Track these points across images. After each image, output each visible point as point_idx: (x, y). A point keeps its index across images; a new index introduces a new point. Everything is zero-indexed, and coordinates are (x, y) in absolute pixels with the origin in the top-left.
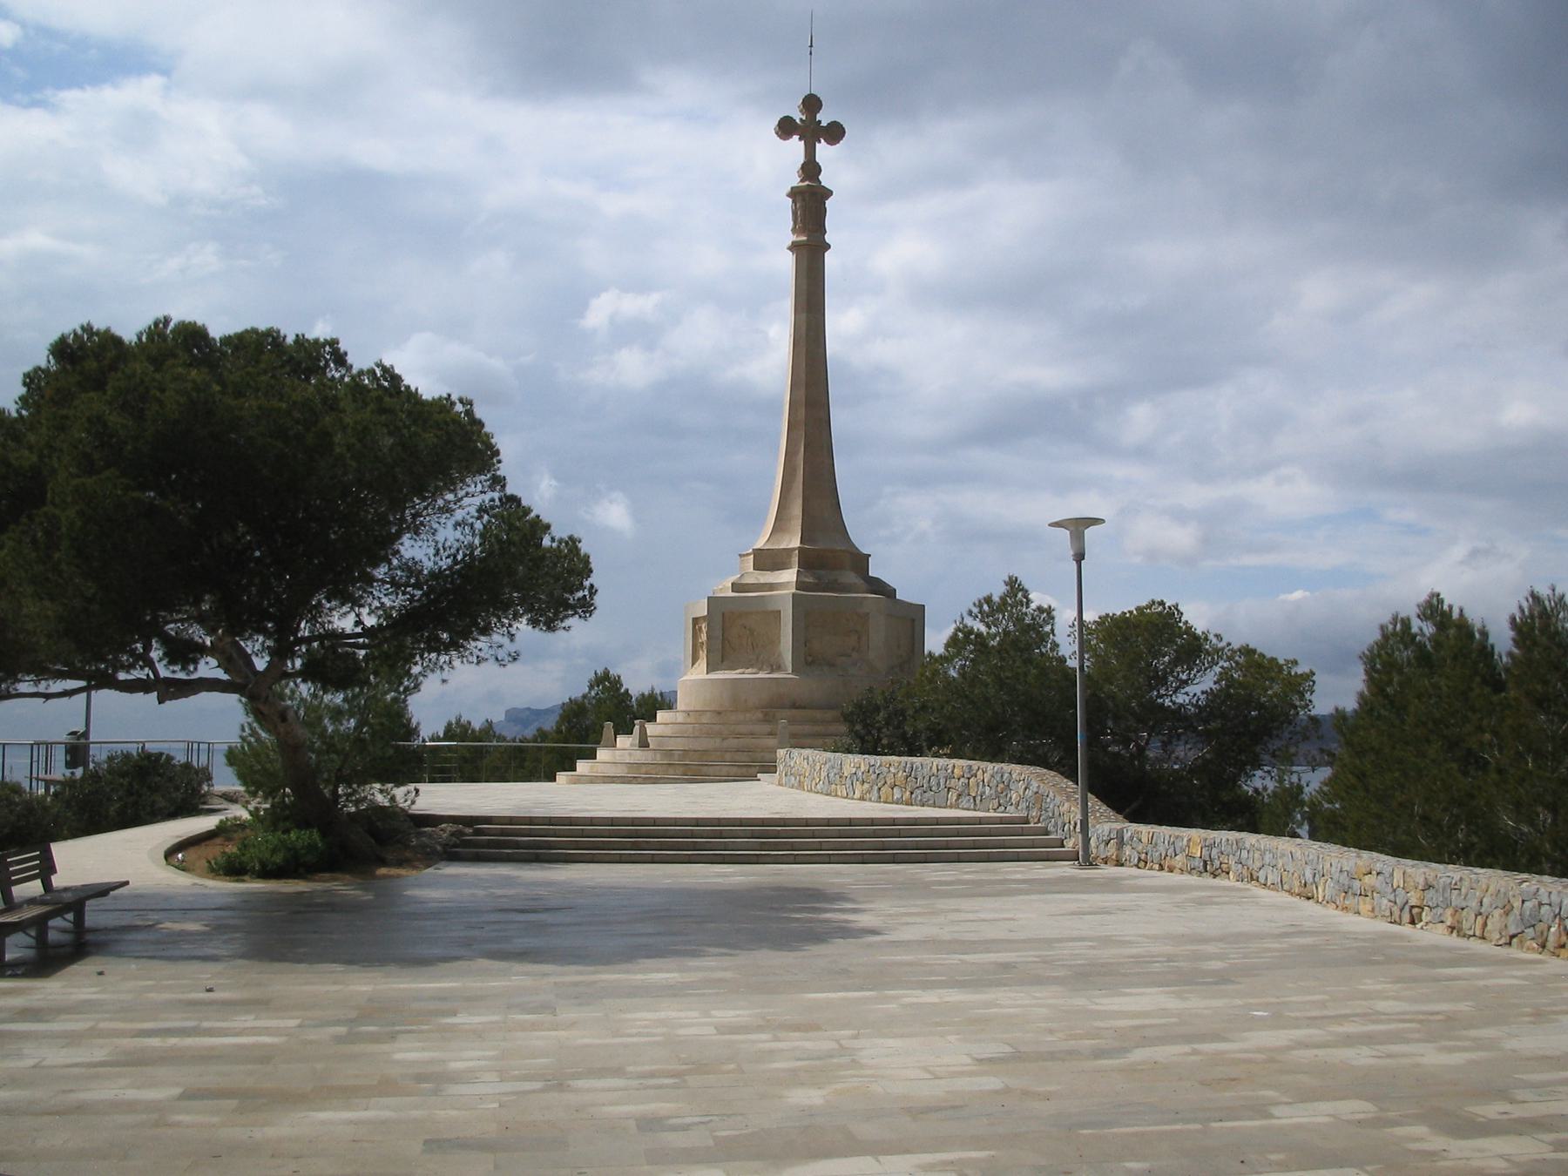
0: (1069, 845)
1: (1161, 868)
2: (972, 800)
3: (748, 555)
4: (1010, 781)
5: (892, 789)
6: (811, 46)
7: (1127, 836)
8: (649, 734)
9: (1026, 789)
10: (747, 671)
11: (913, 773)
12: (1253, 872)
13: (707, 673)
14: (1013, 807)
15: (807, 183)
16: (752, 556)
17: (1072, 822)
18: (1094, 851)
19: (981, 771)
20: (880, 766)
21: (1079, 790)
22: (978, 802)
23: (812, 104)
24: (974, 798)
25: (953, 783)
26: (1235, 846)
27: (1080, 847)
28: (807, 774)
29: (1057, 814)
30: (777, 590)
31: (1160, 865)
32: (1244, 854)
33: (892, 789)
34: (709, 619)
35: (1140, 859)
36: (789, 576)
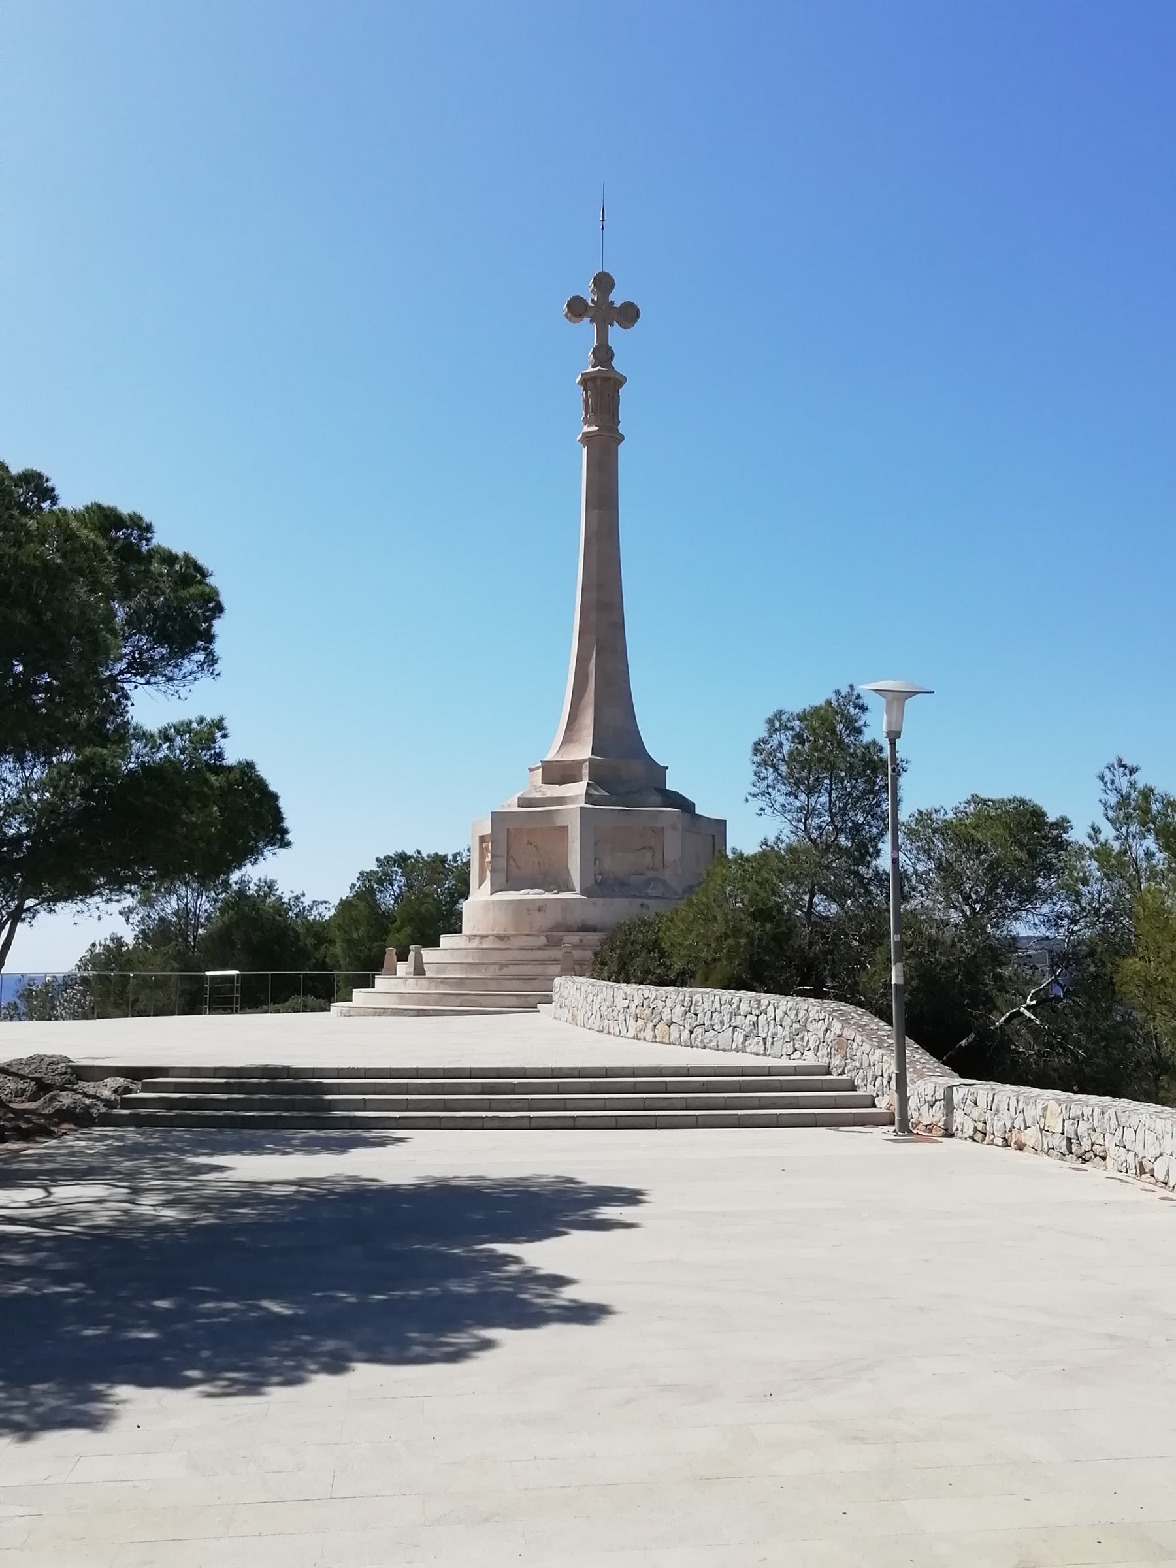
0: (882, 1104)
1: (1006, 1143)
2: (762, 1043)
3: (538, 768)
4: (807, 1019)
5: (669, 1026)
6: (603, 220)
7: (957, 1097)
8: (424, 961)
9: (827, 1030)
10: (532, 891)
11: (692, 1008)
12: (1144, 1161)
13: (491, 894)
14: (811, 1052)
15: (597, 369)
16: (541, 770)
17: (885, 1075)
18: (915, 1115)
19: (771, 1006)
20: (656, 999)
21: (894, 1034)
22: (769, 1044)
23: (604, 283)
24: (764, 1039)
25: (738, 1020)
26: (1113, 1121)
27: (896, 1108)
28: (580, 1007)
29: (865, 1064)
30: (566, 804)
31: (1004, 1139)
32: (1129, 1134)
33: (669, 1026)
34: (493, 837)
35: (976, 1130)
36: (578, 789)
